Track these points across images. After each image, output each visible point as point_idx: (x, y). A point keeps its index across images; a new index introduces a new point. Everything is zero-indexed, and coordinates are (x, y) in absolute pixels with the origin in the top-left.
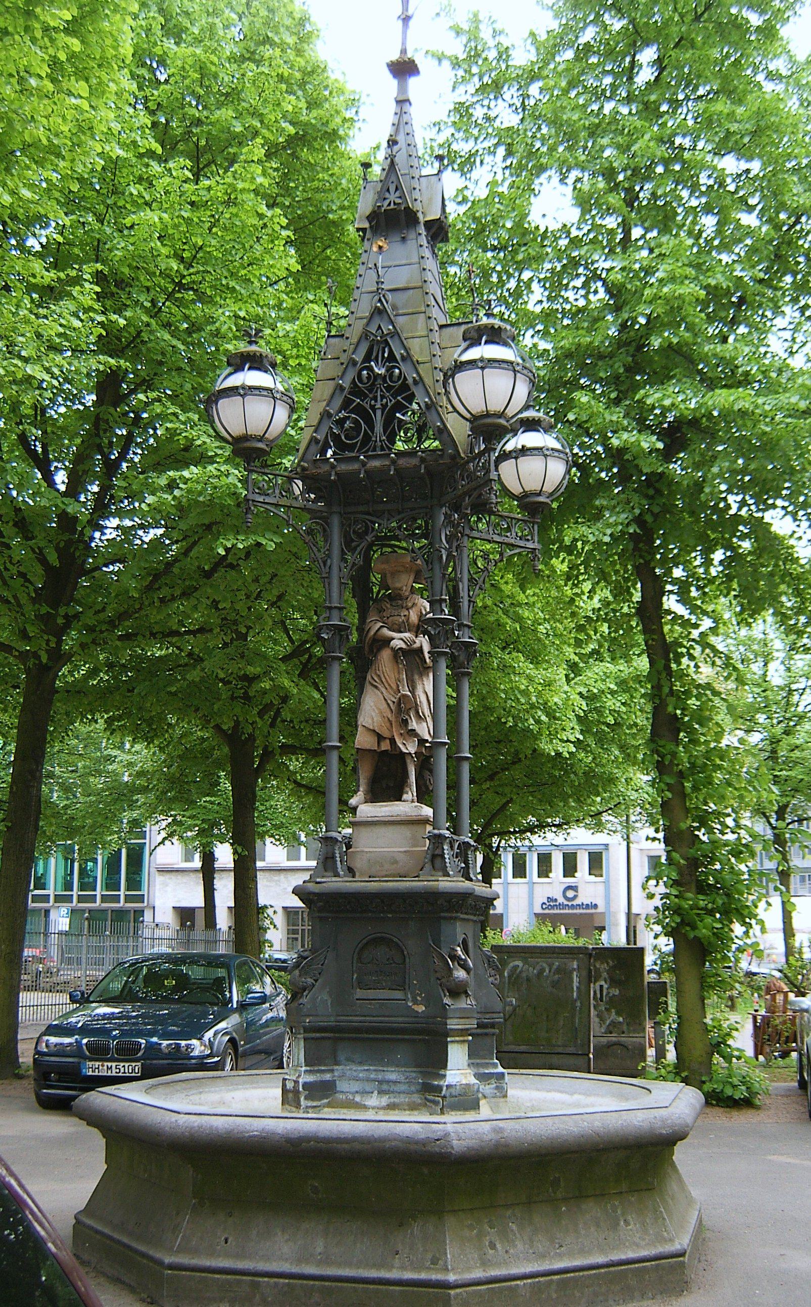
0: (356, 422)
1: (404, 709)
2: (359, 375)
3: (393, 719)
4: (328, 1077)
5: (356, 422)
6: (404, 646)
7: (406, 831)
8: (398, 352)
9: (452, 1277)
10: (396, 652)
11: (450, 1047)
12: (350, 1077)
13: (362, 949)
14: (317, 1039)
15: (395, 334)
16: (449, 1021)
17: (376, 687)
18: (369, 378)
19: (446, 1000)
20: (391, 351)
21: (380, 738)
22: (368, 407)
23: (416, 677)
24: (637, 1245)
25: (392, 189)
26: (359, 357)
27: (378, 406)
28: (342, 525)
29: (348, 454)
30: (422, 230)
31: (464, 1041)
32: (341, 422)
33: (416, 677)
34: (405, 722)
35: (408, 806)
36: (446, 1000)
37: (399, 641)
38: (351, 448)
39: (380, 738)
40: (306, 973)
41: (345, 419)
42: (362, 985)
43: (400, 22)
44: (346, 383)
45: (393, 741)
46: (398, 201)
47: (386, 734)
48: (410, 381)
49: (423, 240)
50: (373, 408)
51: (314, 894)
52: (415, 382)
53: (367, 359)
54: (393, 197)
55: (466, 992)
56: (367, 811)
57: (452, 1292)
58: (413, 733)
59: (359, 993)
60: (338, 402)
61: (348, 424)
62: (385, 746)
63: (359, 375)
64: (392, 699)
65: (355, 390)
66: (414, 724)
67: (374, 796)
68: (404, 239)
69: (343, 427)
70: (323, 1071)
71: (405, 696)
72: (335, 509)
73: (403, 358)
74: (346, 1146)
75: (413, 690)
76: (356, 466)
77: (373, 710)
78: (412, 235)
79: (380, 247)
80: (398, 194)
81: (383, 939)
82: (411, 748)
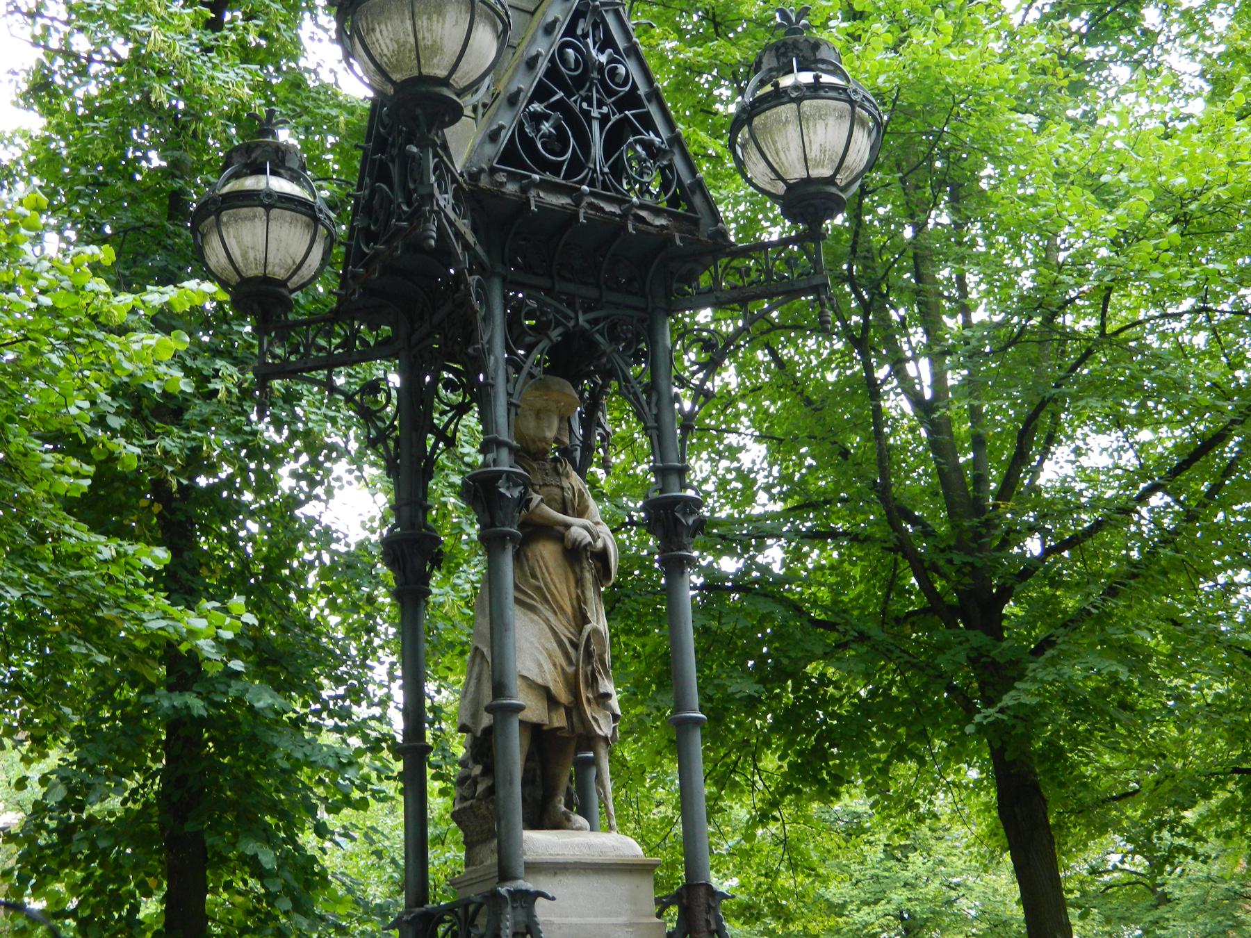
0: (558, 127)
17: (532, 609)
39: (551, 701)
47: (562, 695)
50: (587, 114)
61: (546, 127)
62: (559, 720)
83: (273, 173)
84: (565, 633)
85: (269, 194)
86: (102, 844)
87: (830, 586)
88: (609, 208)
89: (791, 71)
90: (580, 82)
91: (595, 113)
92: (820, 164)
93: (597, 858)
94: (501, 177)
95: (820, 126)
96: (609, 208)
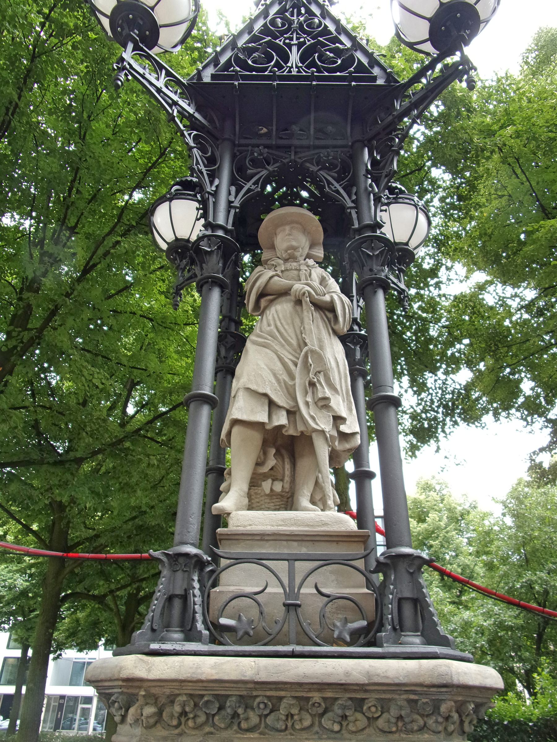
45: (292, 413)
47: (280, 399)
62: (281, 419)
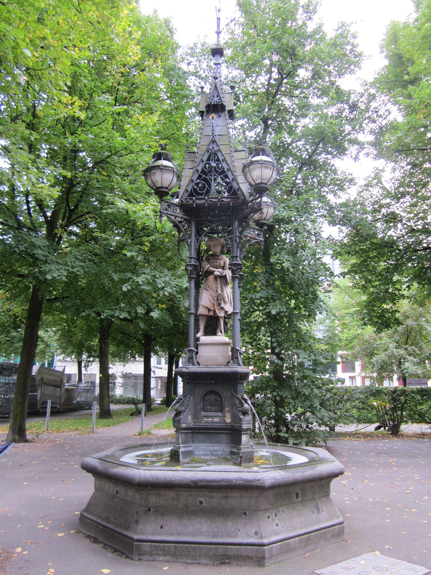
0: (203, 184)
1: (219, 300)
2: (205, 166)
3: (215, 303)
4: (190, 449)
5: (203, 184)
6: (219, 274)
7: (221, 348)
8: (221, 158)
9: (265, 541)
10: (216, 277)
11: (243, 436)
12: (201, 448)
13: (204, 396)
14: (186, 433)
15: (220, 151)
16: (243, 425)
17: (207, 290)
18: (209, 167)
19: (242, 417)
20: (218, 157)
21: (209, 310)
22: (208, 178)
23: (224, 287)
24: (327, 520)
25: (216, 96)
26: (205, 159)
27: (213, 178)
28: (196, 226)
29: (200, 197)
30: (226, 113)
31: (247, 433)
32: (197, 184)
33: (224, 287)
34: (219, 304)
35: (221, 337)
36: (242, 417)
37: (217, 272)
38: (201, 194)
39: (209, 310)
40: (182, 405)
41: (200, 183)
42: (205, 410)
43: (216, 35)
44: (200, 169)
45: (214, 311)
46: (218, 101)
47: (212, 308)
48: (226, 170)
49: (227, 117)
50: (211, 179)
51: (186, 373)
52: (228, 170)
53: (208, 160)
54: (216, 99)
55: (248, 413)
56: (204, 339)
57: (265, 548)
58: (222, 308)
59: (203, 414)
60: (196, 176)
61: (200, 185)
62: (211, 313)
63: (205, 166)
64: (214, 295)
65: (203, 172)
66: (223, 305)
67: (206, 333)
68: (219, 116)
69: (198, 186)
70: (188, 447)
71: (220, 294)
72: (193, 219)
73: (223, 161)
74: (218, 484)
75: (222, 291)
76: (204, 201)
77: (206, 299)
78: (223, 115)
79: (213, 117)
80: (218, 98)
81: (213, 391)
82: (221, 314)
83: (262, 155)
84: (214, 295)
85: (261, 161)
86: (275, 345)
87: (66, 321)
88: (214, 200)
89: (260, 155)
90: (210, 172)
91: (213, 178)
92: (257, 180)
93: (216, 342)
94: (188, 200)
95: (255, 171)
96: (214, 200)
